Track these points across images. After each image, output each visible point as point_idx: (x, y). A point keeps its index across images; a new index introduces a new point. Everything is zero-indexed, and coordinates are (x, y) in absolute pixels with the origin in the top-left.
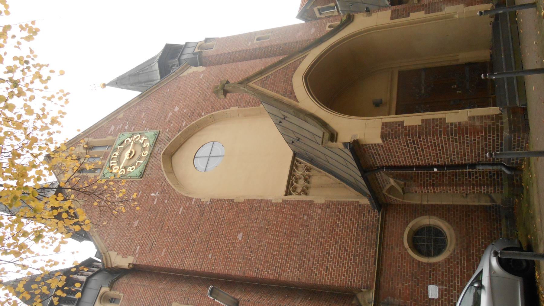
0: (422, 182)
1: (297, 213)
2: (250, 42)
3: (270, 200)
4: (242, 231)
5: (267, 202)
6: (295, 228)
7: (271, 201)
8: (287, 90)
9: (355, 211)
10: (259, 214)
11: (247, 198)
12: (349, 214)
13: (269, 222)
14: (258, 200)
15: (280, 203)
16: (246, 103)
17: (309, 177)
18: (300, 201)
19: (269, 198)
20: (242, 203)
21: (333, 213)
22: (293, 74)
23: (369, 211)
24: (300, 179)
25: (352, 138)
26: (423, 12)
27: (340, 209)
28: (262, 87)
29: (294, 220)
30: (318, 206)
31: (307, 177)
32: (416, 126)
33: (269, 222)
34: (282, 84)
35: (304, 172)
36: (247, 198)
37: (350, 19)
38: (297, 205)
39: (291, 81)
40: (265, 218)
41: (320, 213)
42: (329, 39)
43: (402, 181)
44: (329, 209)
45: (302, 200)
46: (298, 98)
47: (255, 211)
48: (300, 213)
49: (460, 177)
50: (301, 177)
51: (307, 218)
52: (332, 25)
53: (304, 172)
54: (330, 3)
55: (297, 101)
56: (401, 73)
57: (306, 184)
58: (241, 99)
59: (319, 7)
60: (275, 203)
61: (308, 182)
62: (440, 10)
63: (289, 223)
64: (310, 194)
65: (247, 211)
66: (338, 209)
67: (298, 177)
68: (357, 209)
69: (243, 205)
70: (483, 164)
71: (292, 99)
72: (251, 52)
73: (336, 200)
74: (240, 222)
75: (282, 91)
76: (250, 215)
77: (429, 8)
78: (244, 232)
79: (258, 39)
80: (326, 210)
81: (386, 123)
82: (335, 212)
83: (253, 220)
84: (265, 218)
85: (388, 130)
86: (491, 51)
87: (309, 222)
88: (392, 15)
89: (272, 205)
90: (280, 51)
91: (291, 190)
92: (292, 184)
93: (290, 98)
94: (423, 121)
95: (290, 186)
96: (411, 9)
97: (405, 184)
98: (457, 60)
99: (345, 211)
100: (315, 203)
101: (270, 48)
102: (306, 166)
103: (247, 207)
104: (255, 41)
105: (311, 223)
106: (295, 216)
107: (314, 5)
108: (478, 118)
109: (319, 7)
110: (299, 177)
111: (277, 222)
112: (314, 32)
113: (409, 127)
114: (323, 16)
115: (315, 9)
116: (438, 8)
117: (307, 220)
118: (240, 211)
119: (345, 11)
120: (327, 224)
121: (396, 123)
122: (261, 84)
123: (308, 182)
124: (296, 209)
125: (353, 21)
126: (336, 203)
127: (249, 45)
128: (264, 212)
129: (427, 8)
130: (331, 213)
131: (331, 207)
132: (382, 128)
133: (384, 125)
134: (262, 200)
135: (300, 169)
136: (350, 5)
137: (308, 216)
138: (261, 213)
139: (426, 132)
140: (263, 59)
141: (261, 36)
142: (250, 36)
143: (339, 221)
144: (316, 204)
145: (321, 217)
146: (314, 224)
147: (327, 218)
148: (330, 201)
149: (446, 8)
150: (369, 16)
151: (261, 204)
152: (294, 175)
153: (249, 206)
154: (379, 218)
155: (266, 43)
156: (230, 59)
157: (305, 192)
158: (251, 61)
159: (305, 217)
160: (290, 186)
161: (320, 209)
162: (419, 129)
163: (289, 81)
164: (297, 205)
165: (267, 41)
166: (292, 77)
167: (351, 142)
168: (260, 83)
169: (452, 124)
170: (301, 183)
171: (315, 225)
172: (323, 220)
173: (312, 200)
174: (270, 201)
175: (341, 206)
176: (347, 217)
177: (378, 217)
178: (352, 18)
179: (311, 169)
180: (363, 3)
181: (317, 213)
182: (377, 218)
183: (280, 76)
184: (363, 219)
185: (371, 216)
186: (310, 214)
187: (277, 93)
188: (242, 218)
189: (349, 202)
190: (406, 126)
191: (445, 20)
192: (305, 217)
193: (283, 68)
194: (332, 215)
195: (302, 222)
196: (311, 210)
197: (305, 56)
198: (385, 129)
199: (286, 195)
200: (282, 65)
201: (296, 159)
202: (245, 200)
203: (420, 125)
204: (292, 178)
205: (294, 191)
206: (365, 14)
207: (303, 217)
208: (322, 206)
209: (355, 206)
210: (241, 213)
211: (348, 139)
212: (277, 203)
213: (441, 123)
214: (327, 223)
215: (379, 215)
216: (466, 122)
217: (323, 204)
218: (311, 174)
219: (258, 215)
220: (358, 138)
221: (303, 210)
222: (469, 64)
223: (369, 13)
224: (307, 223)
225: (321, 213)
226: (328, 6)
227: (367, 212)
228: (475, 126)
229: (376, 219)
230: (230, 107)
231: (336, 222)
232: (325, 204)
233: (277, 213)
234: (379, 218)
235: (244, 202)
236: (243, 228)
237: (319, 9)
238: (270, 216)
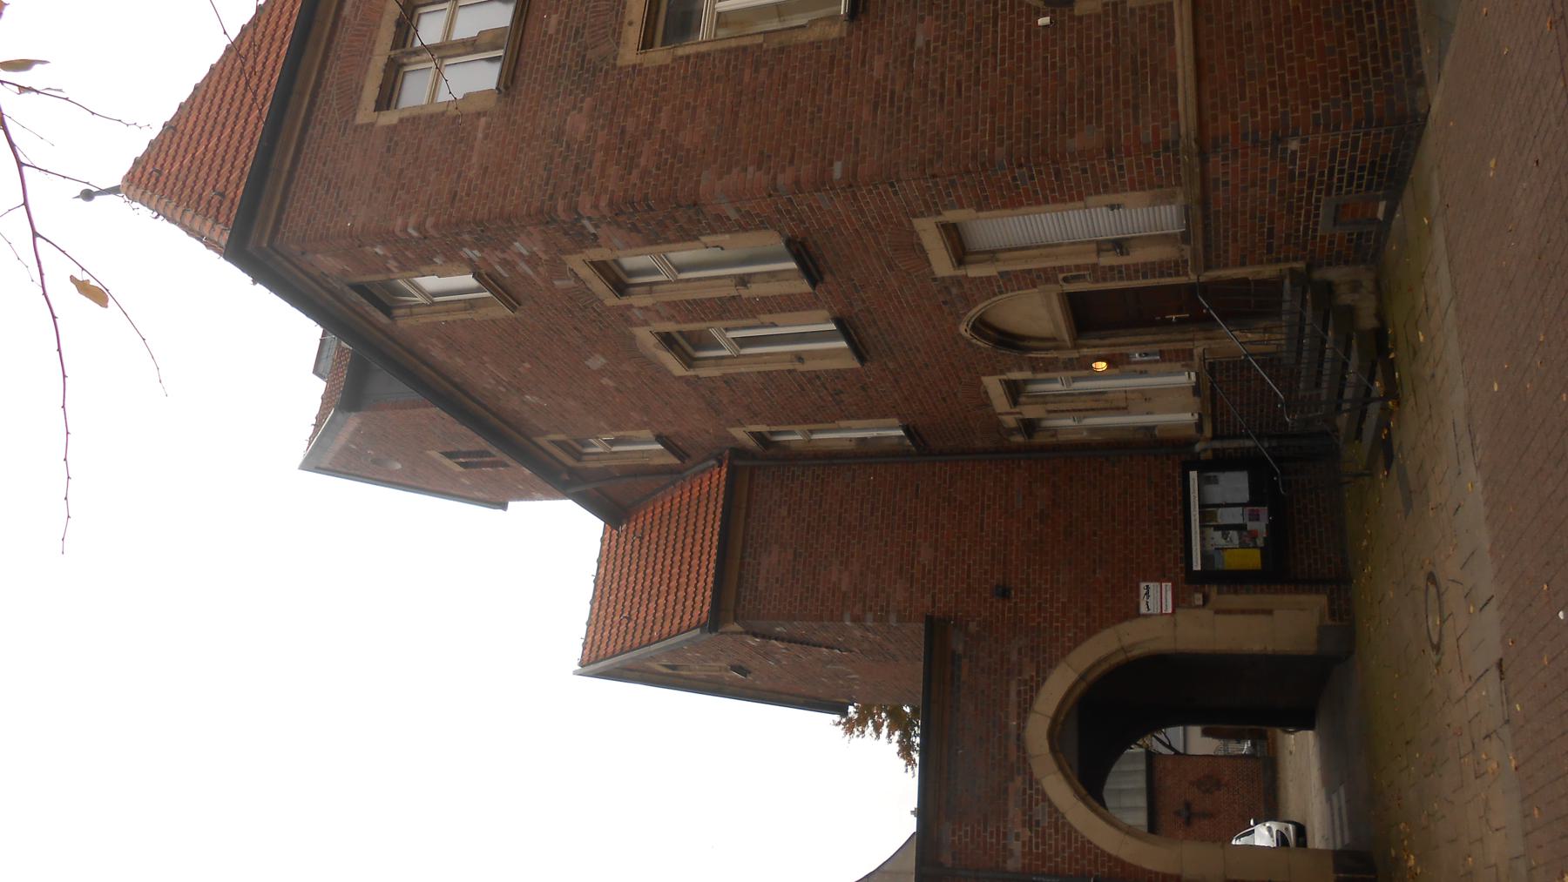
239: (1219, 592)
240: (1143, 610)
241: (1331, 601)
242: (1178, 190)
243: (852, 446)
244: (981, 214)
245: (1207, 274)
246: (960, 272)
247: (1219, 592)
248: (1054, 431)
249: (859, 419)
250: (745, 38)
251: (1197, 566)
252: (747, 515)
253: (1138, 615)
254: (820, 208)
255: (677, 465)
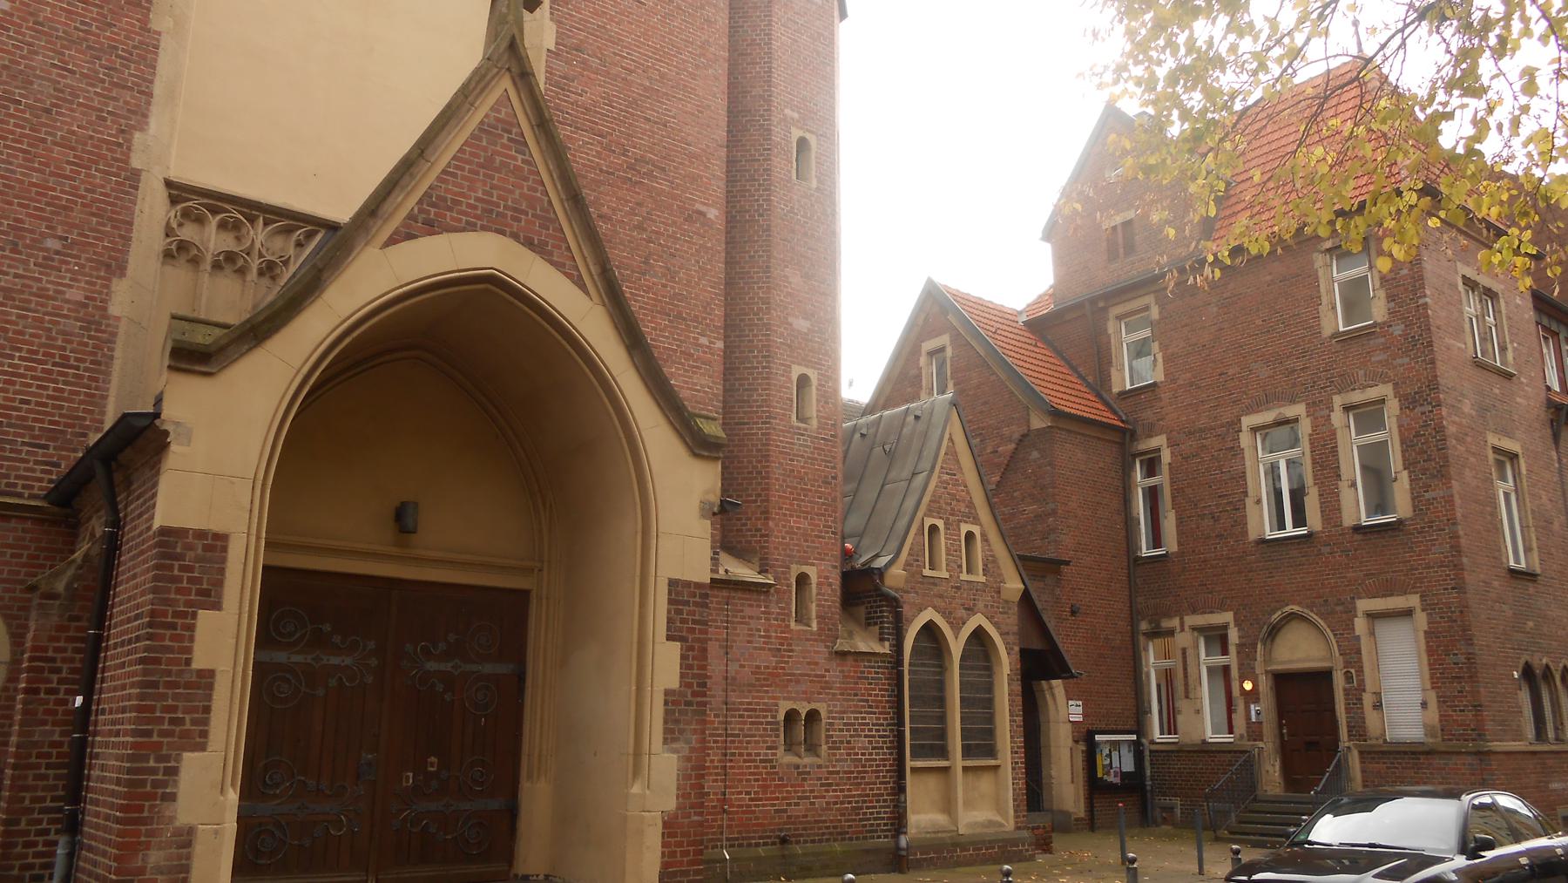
0: (50, 654)
1: (77, 215)
2: (796, 115)
3: (147, 124)
4: (18, 10)
5: (139, 115)
6: (10, 203)
7: (142, 130)
8: (450, 209)
9: (61, 416)
10: (91, 78)
11: (167, 44)
12: (49, 397)
13: (48, 111)
14: (151, 82)
15: (126, 162)
16: (565, 78)
17: (242, 272)
18: (130, 231)
19: (153, 123)
20: (144, 22)
21: (59, 343)
22: (515, 236)
23: (57, 465)
24: (238, 239)
25: (178, 424)
26: (674, 683)
27: (78, 368)
28: (482, 122)
29: (48, 204)
30: (100, 293)
31: (240, 263)
32: (189, 650)
33: (48, 111)
34: (480, 195)
35: (261, 255)
36: (162, 45)
37: (699, 445)
38: (110, 219)
39: (484, 228)
40: (64, 100)
41: (67, 296)
42: (637, 370)
43: (68, 586)
44: (81, 328)
45: (130, 239)
46: (406, 246)
47: (101, 66)
48: (73, 226)
49: (54, 779)
50: (243, 241)
51: (47, 250)
52: (810, 386)
53: (261, 255)
54: (955, 385)
55: (392, 241)
56: (522, 597)
57: (209, 258)
58: (584, 62)
59: (949, 352)
60: (129, 141)
61: (217, 266)
62: (670, 736)
63: (35, 185)
64: (168, 269)
65: (109, 38)
66: (77, 359)
67: (244, 231)
68: (66, 425)
69: (133, 25)
70: (71, 856)
71: (404, 224)
72: (762, 116)
73: (118, 353)
74: (62, 9)
75: (447, 190)
76: (89, 47)
77: (688, 704)
78: (12, 15)
79: (802, 144)
80: (77, 319)
81: (225, 549)
82: (64, 349)
83: (63, 54)
84: (64, 100)
85: (190, 554)
86: (541, 877)
87: (31, 255)
88: (688, 584)
89: (123, 131)
90: (748, 211)
91: (190, 204)
92: (215, 211)
93: (411, 217)
94: (207, 678)
95: (206, 201)
96: (696, 645)
97: (53, 596)
98: (530, 777)
99: (65, 383)
100: (115, 281)
101: (764, 180)
102: (286, 263)
103: (127, 37)
104: (796, 133)
105: (25, 262)
106: (65, 208)
107: (956, 337)
108: (180, 858)
109: (949, 352)
110: (243, 236)
111: (44, 141)
112: (795, 326)
113: (191, 628)
114: (923, 360)
115: (944, 340)
116: (681, 732)
117: (42, 249)
118: (111, 11)
119: (877, 431)
120: (14, 318)
121: (220, 583)
122: (498, 120)
123: (217, 266)
124: (94, 215)
125: (696, 455)
126: (104, 355)
127: (787, 111)
128: (96, 99)
129: (689, 698)
130: (64, 333)
131: (90, 337)
132: (201, 534)
133: (216, 543)
134: (150, 95)
135: (278, 242)
136: (887, 448)
137: (57, 253)
138: (93, 86)
139: (154, 685)
140: (723, 153)
141: (813, 156)
142: (821, 117)
143: (21, 358)
144: (107, 287)
145: (49, 298)
146: (21, 272)
147: (41, 321)
148: (114, 334)
149: (675, 756)
150: (702, 509)
151: (132, 89)
152: (252, 220)
153: (127, 45)
154: (20, 495)
155: (783, 167)
156: (751, 45)
157: (178, 252)
158: (725, 113)
159: (52, 244)
160: (206, 201)
161: (87, 298)
162: (176, 662)
163: (489, 220)
164: (110, 219)
165: (790, 172)
166: (503, 233)
167: (157, 422)
168: (502, 116)
169: (174, 771)
170: (213, 239)
171: (16, 276)
172: (33, 306)
173: (129, 272)
174: (142, 126)
175: (86, 369)
176: (39, 387)
177: (26, 493)
178: (706, 454)
179: (273, 278)
180: (883, 486)
181: (70, 287)
182: (19, 489)
183: (517, 192)
184: (24, 443)
185: (33, 471)
186: (67, 263)
187: (444, 172)
188: (77, 14)
189: (105, 398)
190: (194, 615)
191: (631, 751)
192: (52, 244)
193: (550, 202)
194: (55, 339)
195: (32, 232)
196: (82, 266)
197: (583, 287)
198: (199, 544)
199: (169, 184)
200: (561, 201)
201: (316, 232)
202: (159, 33)
203: (188, 662)
204: (240, 212)
205: (186, 214)
206: (715, 498)
207: (55, 237)
208: (96, 307)
209: (84, 419)
210: (98, 14)
211: (172, 412)
212: (129, 149)
213: (186, 735)
214: (19, 316)
215: (32, 497)
216: (172, 819)
217: (105, 309)
218: (249, 278)
219: (83, 74)
220: (174, 447)
221: (87, 237)
222: (512, 813)
223: (716, 509)
224: (27, 247)
225: (68, 301)
226: (949, 377)
227: (52, 456)
228: (148, 849)
229: (15, 485)
230: (559, 23)
231: (20, 350)
232: (107, 317)
233: (85, 144)
234: (20, 495)
235: (149, 31)
236: (31, 14)
237: (942, 349)
238: (74, 118)
239: (1083, 751)
240: (1071, 702)
241: (1082, 819)
242: (1440, 739)
243: (1135, 515)
244: (1421, 635)
245: (1355, 753)
246: (1360, 614)
247: (1083, 751)
248: (1146, 650)
249: (1178, 526)
250: (202, 329)
251: (1098, 738)
252: (1099, 439)
253: (1069, 699)
254: (1434, 545)
255: (822, 351)
